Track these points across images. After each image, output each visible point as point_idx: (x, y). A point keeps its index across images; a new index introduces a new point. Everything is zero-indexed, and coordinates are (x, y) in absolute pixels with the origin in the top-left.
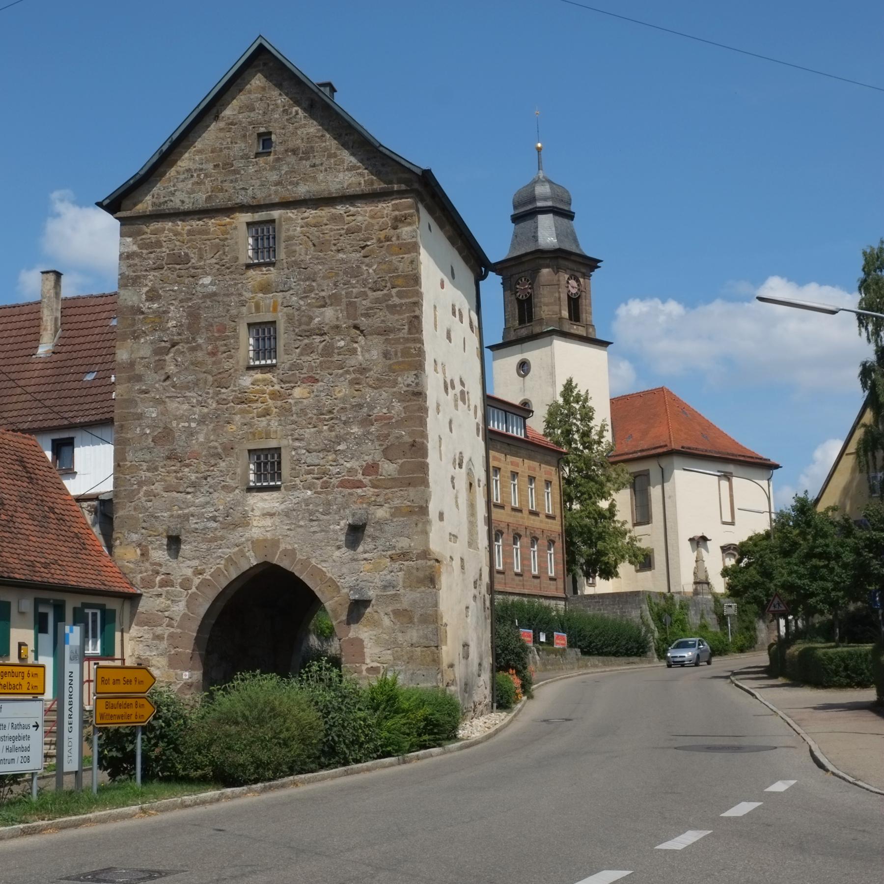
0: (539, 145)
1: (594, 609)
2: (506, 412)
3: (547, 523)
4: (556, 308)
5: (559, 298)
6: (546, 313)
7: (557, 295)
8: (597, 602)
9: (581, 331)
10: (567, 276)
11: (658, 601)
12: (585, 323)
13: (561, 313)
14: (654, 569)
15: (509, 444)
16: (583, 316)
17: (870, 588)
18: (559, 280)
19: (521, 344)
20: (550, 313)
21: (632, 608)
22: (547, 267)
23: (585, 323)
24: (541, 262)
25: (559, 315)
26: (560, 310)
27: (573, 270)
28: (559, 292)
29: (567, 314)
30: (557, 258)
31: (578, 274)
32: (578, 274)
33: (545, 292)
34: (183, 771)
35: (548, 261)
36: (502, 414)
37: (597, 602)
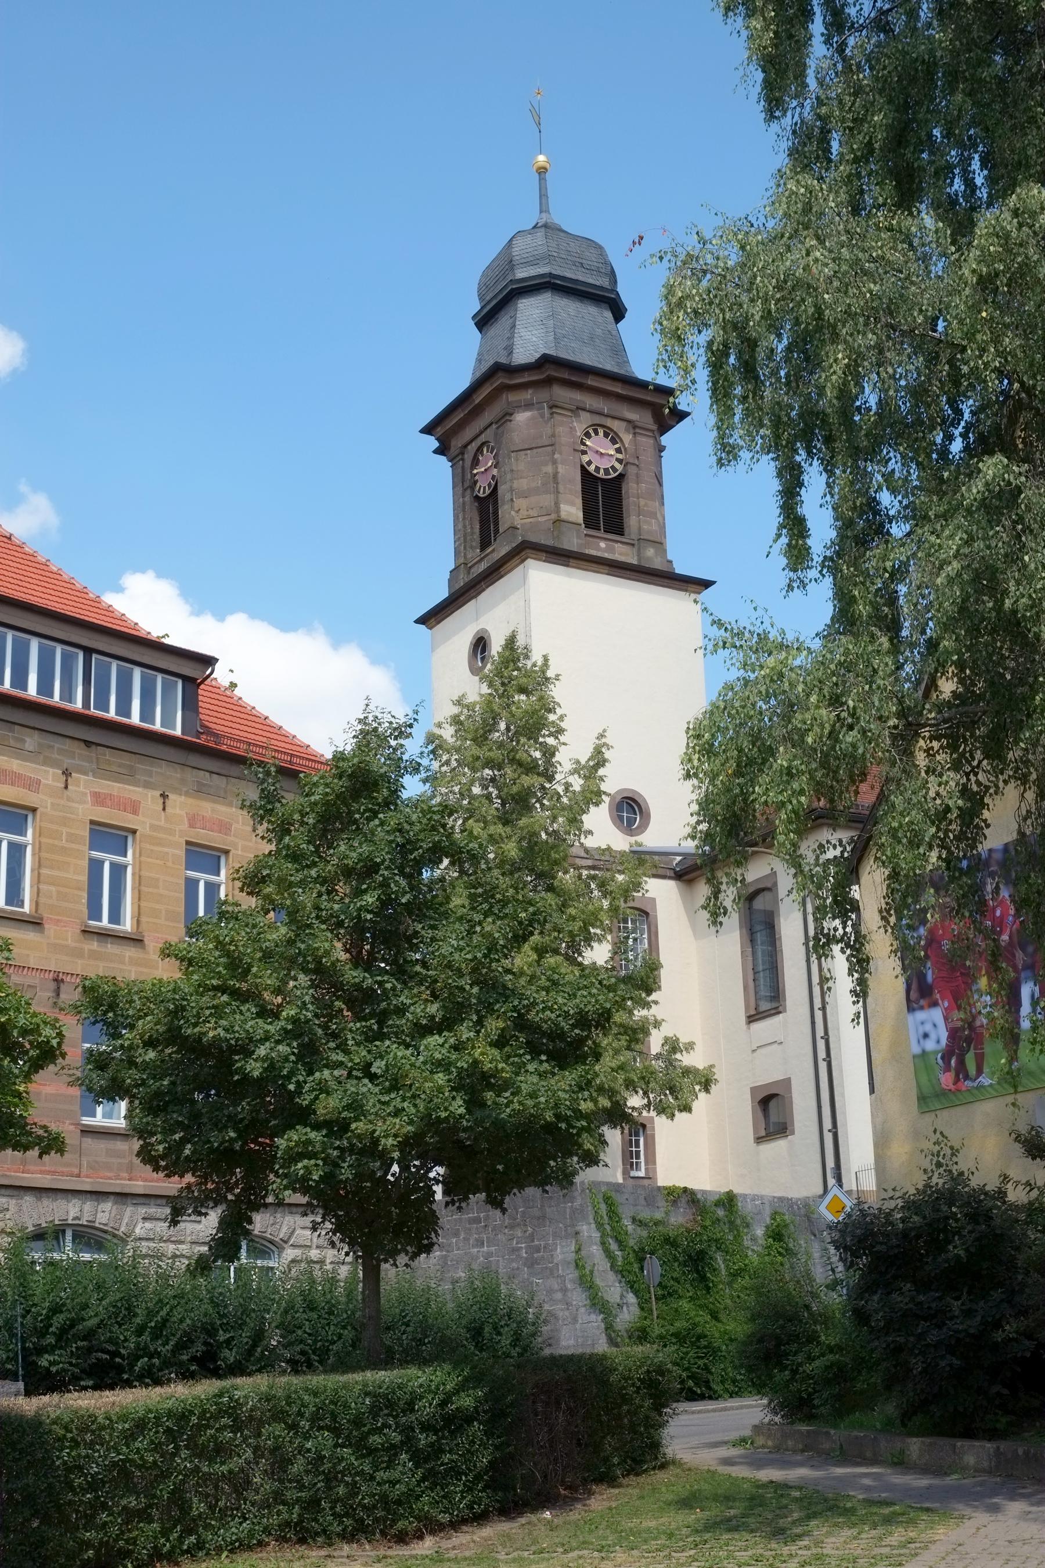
0: (541, 158)
1: (466, 1239)
2: (88, 651)
3: (94, 955)
4: (547, 500)
5: (555, 476)
6: (524, 513)
7: (549, 469)
8: (477, 1220)
9: (621, 553)
10: (579, 428)
11: (659, 1215)
12: (634, 536)
13: (558, 510)
14: (793, 1133)
15: (88, 744)
16: (632, 521)
17: (88, 1045)
18: (553, 436)
19: (475, 597)
20: (532, 513)
21: (556, 1235)
22: (528, 406)
23: (634, 536)
24: (513, 397)
25: (553, 516)
26: (557, 504)
27: (600, 414)
28: (555, 462)
29: (581, 515)
30: (549, 382)
31: (616, 425)
32: (616, 425)
33: (522, 466)
34: (523, 1477)
35: (528, 395)
36: (167, 690)
37: (477, 1220)
